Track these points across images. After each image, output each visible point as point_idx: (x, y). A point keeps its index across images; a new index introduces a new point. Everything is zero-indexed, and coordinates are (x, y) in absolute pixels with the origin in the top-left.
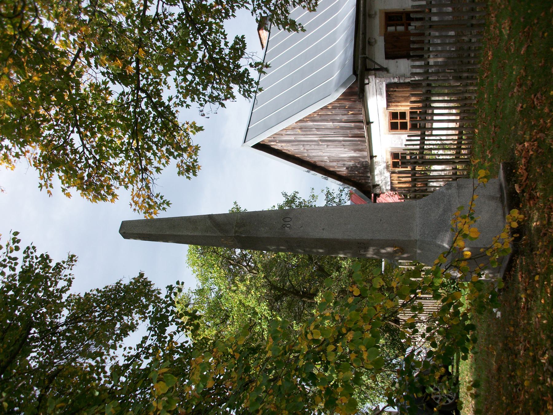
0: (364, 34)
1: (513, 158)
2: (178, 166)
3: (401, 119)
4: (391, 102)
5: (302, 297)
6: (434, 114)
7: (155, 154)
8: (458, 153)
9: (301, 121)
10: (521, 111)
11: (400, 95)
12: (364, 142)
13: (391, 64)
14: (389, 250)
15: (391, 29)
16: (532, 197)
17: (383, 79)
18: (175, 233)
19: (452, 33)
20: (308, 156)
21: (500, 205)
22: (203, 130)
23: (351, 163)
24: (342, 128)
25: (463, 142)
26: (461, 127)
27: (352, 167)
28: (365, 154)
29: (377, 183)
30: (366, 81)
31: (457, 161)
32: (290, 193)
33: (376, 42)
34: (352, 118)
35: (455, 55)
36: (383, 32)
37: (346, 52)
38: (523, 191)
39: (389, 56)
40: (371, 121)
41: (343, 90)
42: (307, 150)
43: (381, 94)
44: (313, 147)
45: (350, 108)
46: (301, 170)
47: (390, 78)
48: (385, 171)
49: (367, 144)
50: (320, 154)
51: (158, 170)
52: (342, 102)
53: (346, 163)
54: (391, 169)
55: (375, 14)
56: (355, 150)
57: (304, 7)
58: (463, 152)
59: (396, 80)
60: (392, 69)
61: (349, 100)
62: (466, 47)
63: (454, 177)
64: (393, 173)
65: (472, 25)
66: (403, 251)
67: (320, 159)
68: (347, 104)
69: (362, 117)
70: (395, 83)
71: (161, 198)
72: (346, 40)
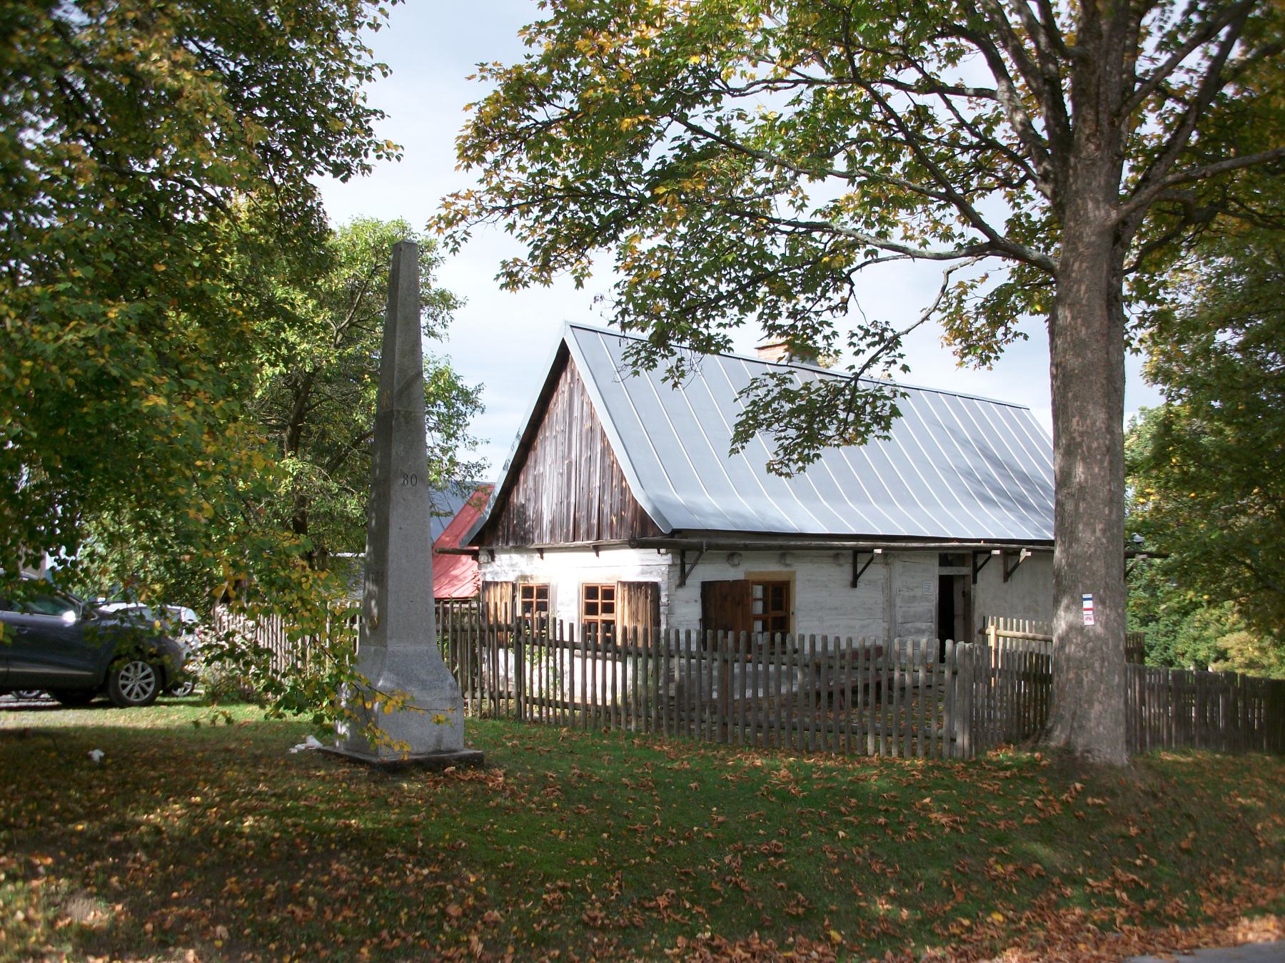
0: (746, 547)
1: (489, 766)
2: (516, 260)
3: (604, 605)
4: (629, 589)
5: (294, 426)
6: (605, 660)
7: (537, 220)
8: (534, 701)
9: (603, 435)
10: (546, 776)
11: (641, 605)
12: (567, 540)
13: (693, 591)
14: (375, 611)
15: (758, 592)
16: (437, 783)
17: (666, 578)
18: (398, 327)
19: (715, 695)
20: (545, 438)
21: (431, 749)
22: (577, 287)
23: (530, 512)
24: (590, 501)
25: (558, 710)
26: (575, 706)
27: (524, 513)
28: (547, 540)
29: (497, 557)
30: (663, 551)
31: (522, 700)
32: (483, 398)
33: (734, 566)
34: (606, 521)
35: (704, 699)
36: (751, 578)
37: (719, 515)
38: (446, 775)
39: (707, 587)
40: (601, 553)
41: (648, 510)
42: (555, 437)
43: (643, 573)
44: (560, 448)
45: (621, 519)
46: (520, 421)
47: (668, 589)
48: (518, 574)
49: (562, 544)
50: (549, 461)
51: (511, 227)
52: (631, 507)
53: (532, 504)
54: (521, 584)
55: (787, 565)
56: (552, 522)
57: (776, 454)
58: (536, 709)
59: (664, 600)
60: (682, 593)
61: (634, 519)
62: (695, 715)
63: (496, 694)
64: (514, 586)
65: (725, 725)
66: (374, 628)
67: (540, 460)
68: (628, 515)
69: (606, 538)
70: (659, 598)
71: (464, 239)
72: (740, 516)
